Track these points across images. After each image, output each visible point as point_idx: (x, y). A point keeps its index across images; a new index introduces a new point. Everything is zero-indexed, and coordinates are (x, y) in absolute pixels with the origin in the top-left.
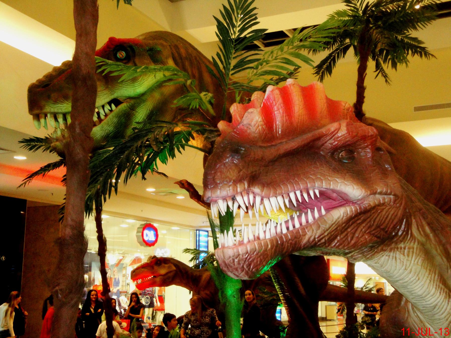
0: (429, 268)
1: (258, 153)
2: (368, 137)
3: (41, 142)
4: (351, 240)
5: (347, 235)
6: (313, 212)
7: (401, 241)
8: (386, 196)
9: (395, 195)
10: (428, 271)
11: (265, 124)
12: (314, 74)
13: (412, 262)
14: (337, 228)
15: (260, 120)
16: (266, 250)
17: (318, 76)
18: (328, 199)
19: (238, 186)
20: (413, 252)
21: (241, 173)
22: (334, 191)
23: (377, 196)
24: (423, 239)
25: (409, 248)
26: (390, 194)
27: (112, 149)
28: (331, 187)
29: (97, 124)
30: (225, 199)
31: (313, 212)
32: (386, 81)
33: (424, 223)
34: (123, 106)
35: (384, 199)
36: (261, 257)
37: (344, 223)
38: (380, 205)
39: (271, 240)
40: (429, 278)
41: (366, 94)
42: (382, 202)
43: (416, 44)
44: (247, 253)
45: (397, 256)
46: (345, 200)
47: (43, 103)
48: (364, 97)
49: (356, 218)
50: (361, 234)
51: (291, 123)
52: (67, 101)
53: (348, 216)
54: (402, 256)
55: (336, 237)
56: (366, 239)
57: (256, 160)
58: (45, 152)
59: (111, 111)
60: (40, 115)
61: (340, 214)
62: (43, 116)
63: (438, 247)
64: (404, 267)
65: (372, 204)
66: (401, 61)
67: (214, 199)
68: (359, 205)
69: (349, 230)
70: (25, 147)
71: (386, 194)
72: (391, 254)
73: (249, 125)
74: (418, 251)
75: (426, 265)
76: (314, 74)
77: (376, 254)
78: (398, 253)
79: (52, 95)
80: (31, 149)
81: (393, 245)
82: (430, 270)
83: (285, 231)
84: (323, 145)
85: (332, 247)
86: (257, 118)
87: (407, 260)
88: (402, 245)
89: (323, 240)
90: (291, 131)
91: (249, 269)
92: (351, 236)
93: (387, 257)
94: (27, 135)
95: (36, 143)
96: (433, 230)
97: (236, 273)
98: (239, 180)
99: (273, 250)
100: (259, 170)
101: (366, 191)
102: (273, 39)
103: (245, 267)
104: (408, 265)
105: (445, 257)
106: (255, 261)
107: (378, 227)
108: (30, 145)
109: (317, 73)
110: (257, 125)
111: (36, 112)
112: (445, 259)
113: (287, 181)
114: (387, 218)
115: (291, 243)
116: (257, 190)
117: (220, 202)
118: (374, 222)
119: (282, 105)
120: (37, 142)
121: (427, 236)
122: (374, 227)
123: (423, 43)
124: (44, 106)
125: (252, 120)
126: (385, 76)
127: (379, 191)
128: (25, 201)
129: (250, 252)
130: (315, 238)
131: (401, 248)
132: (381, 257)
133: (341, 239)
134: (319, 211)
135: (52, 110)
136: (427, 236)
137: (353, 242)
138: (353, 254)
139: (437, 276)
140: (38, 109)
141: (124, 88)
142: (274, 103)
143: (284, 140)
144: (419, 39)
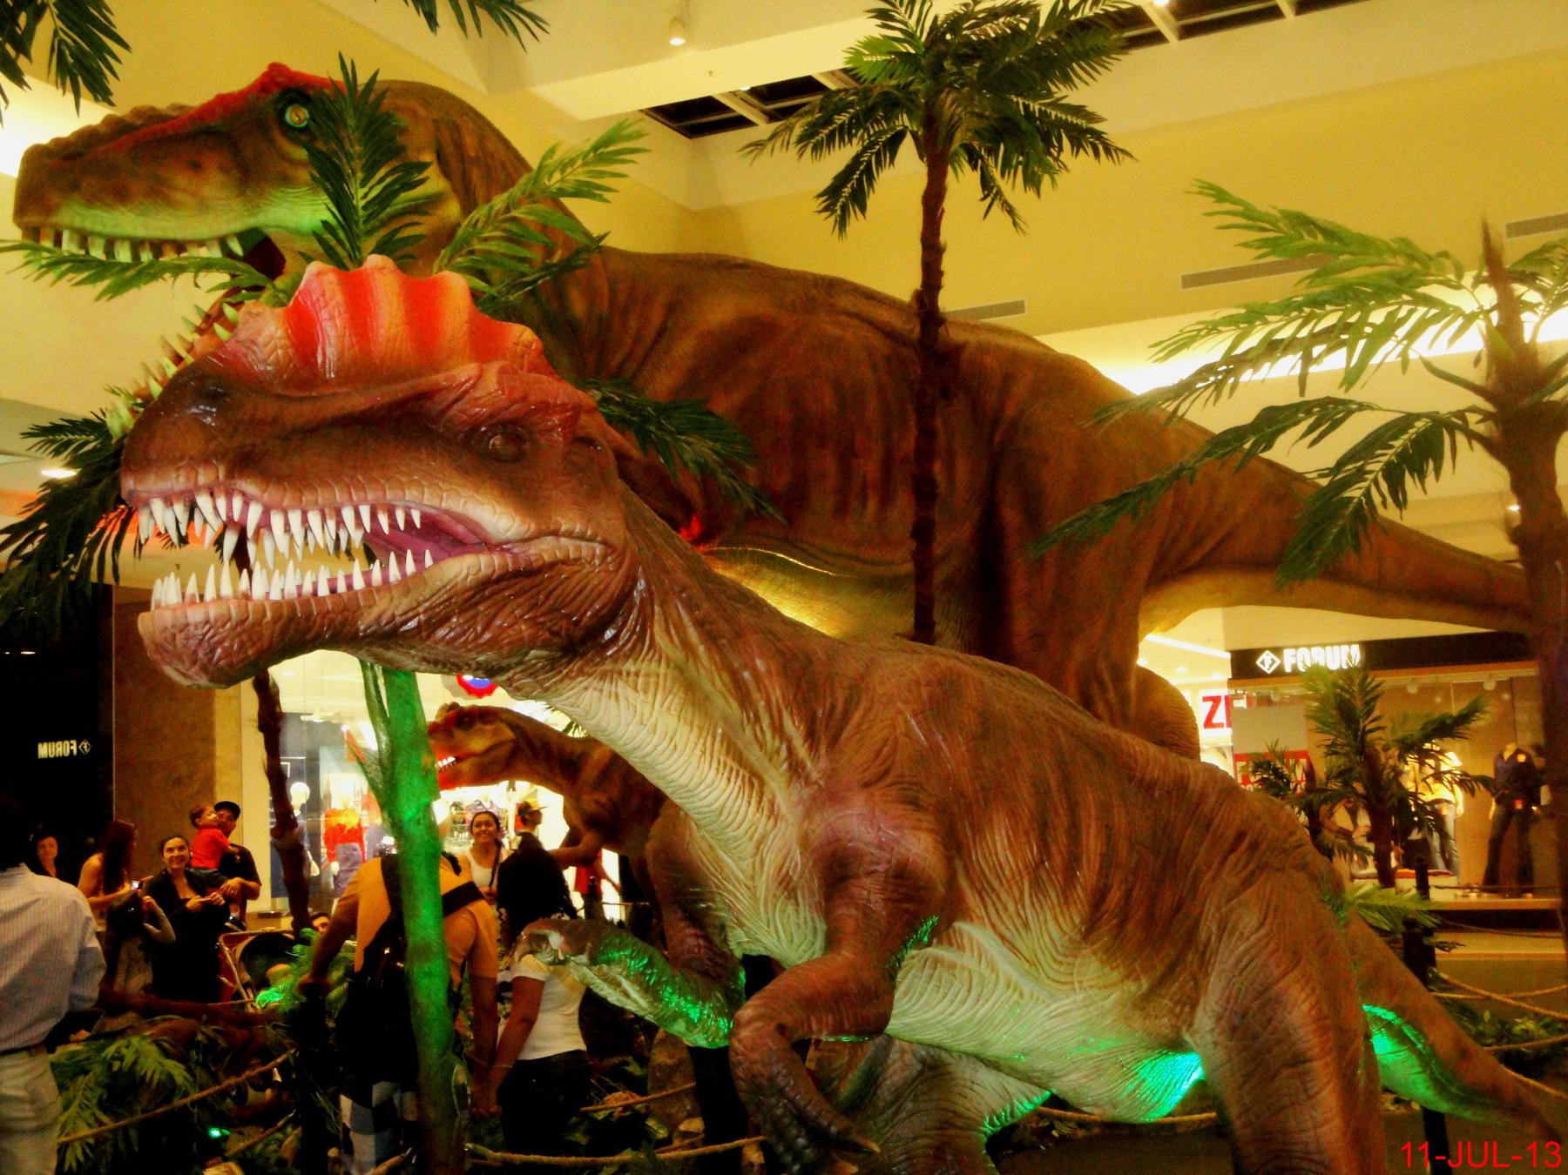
0: (696, 722)
1: (266, 408)
2: (556, 405)
4: (483, 632)
5: (474, 617)
6: (401, 560)
7: (627, 657)
8: (583, 544)
9: (604, 543)
10: (696, 730)
11: (293, 345)
13: (657, 705)
14: (449, 599)
15: (280, 333)
16: (258, 623)
17: (832, 219)
18: (440, 534)
19: (201, 470)
20: (657, 684)
21: (212, 446)
22: (446, 512)
23: (563, 540)
24: (678, 655)
25: (647, 675)
26: (591, 540)
28: (444, 505)
30: (169, 501)
31: (401, 560)
32: (1015, 223)
33: (686, 618)
35: (578, 549)
36: (245, 637)
37: (471, 589)
38: (565, 561)
39: (276, 605)
40: (700, 746)
41: (947, 263)
42: (572, 556)
43: (1083, 123)
44: (207, 622)
45: (620, 690)
46: (486, 544)
48: (941, 274)
49: (503, 584)
50: (514, 622)
51: (368, 353)
53: (481, 575)
54: (630, 691)
55: (447, 619)
56: (521, 631)
57: (255, 424)
61: (463, 569)
63: (717, 678)
64: (638, 718)
65: (547, 558)
66: (1049, 170)
67: (143, 495)
68: (515, 556)
69: (481, 608)
71: (582, 537)
72: (606, 686)
73: (254, 342)
74: (669, 683)
75: (689, 717)
77: (567, 682)
78: (620, 683)
81: (608, 666)
82: (701, 729)
83: (324, 591)
84: (443, 412)
85: (437, 643)
86: (273, 328)
87: (644, 702)
88: (630, 666)
89: (412, 624)
90: (359, 371)
91: (210, 660)
92: (485, 620)
93: (596, 694)
94: (51, 411)
96: (711, 638)
97: (180, 667)
98: (206, 460)
99: (278, 627)
100: (264, 443)
101: (524, 522)
103: (201, 655)
104: (646, 716)
105: (736, 699)
106: (226, 644)
107: (554, 610)
110: (271, 345)
111: (33, 219)
112: (735, 705)
113: (1464, 774)
114: (581, 591)
115: (332, 620)
116: (250, 487)
117: (157, 505)
118: (547, 598)
119: (342, 309)
121: (687, 646)
122: (543, 609)
123: (1100, 120)
124: (58, 206)
125: (259, 333)
126: (1010, 211)
127: (563, 528)
129: (216, 621)
130: (393, 617)
131: (628, 674)
132: (581, 692)
133: (459, 625)
134: (419, 560)
135: (78, 223)
136: (687, 646)
137: (487, 636)
138: (510, 674)
139: (717, 745)
142: (322, 303)
143: (344, 390)
144: (1089, 109)
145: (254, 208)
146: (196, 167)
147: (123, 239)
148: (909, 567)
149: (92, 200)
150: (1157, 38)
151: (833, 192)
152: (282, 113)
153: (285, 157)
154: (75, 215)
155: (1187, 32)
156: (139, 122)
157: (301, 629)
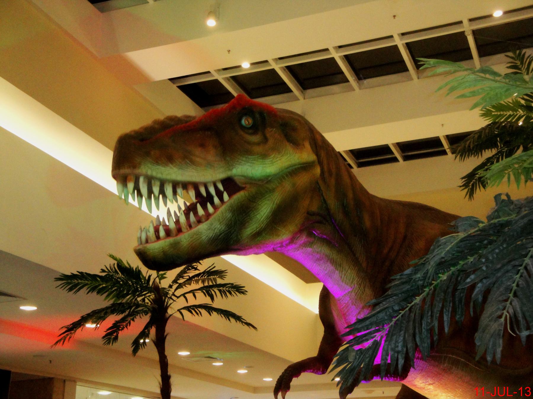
3: (86, 279)
12: (460, 187)
17: (466, 190)
27: (516, 94)
29: (203, 220)
34: (240, 196)
47: (138, 160)
52: (172, 164)
58: (90, 293)
59: (208, 216)
60: (129, 178)
62: (133, 179)
70: (63, 286)
76: (460, 187)
79: (152, 153)
80: (70, 289)
95: (80, 281)
102: (368, 157)
108: (70, 283)
109: (466, 185)
111: (125, 171)
120: (81, 280)
124: (140, 164)
128: (8, 373)
135: (149, 173)
140: (129, 167)
141: (249, 164)
145: (230, 166)
146: (202, 146)
147: (169, 181)
148: (353, 320)
149: (157, 161)
150: (395, 160)
151: (470, 177)
152: (240, 120)
153: (249, 143)
154: (148, 169)
155: (406, 158)
156: (173, 123)
157: (495, 249)
